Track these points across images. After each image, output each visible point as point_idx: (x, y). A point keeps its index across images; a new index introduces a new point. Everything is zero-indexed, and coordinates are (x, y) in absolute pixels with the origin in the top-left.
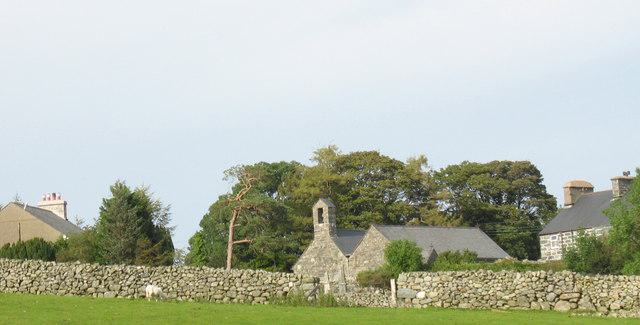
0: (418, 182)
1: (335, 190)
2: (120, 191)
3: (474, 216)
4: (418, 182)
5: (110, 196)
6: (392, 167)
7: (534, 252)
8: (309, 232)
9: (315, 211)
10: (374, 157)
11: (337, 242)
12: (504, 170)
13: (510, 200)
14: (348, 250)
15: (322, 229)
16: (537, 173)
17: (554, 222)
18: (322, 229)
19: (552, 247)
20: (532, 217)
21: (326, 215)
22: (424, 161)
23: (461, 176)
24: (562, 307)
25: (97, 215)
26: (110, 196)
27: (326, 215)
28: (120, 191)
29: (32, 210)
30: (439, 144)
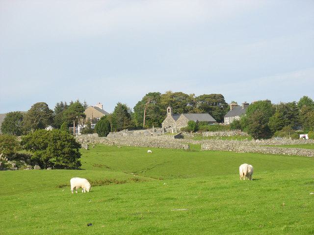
0: (193, 101)
1: (171, 103)
2: (119, 104)
3: (207, 109)
4: (193, 101)
5: (117, 106)
6: (186, 96)
7: (222, 120)
8: (165, 114)
9: (167, 109)
10: (181, 93)
11: (174, 118)
12: (214, 96)
13: (216, 105)
14: (176, 120)
15: (169, 114)
16: (223, 97)
17: (228, 113)
18: (169, 114)
19: (228, 121)
20: (222, 109)
21: (170, 111)
22: (194, 95)
23: (204, 98)
24: (230, 150)
25: (114, 110)
26: (117, 106)
27: (170, 111)
28: (119, 104)
29: (95, 108)
30: (197, 90)
